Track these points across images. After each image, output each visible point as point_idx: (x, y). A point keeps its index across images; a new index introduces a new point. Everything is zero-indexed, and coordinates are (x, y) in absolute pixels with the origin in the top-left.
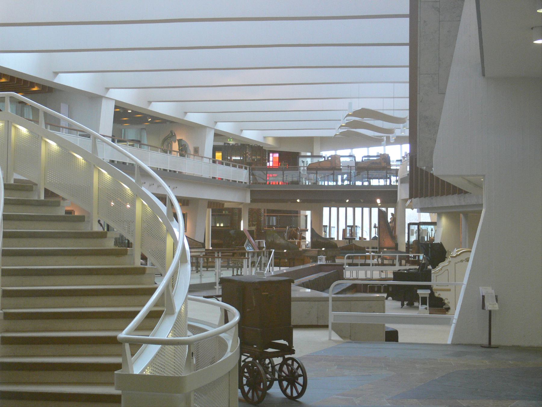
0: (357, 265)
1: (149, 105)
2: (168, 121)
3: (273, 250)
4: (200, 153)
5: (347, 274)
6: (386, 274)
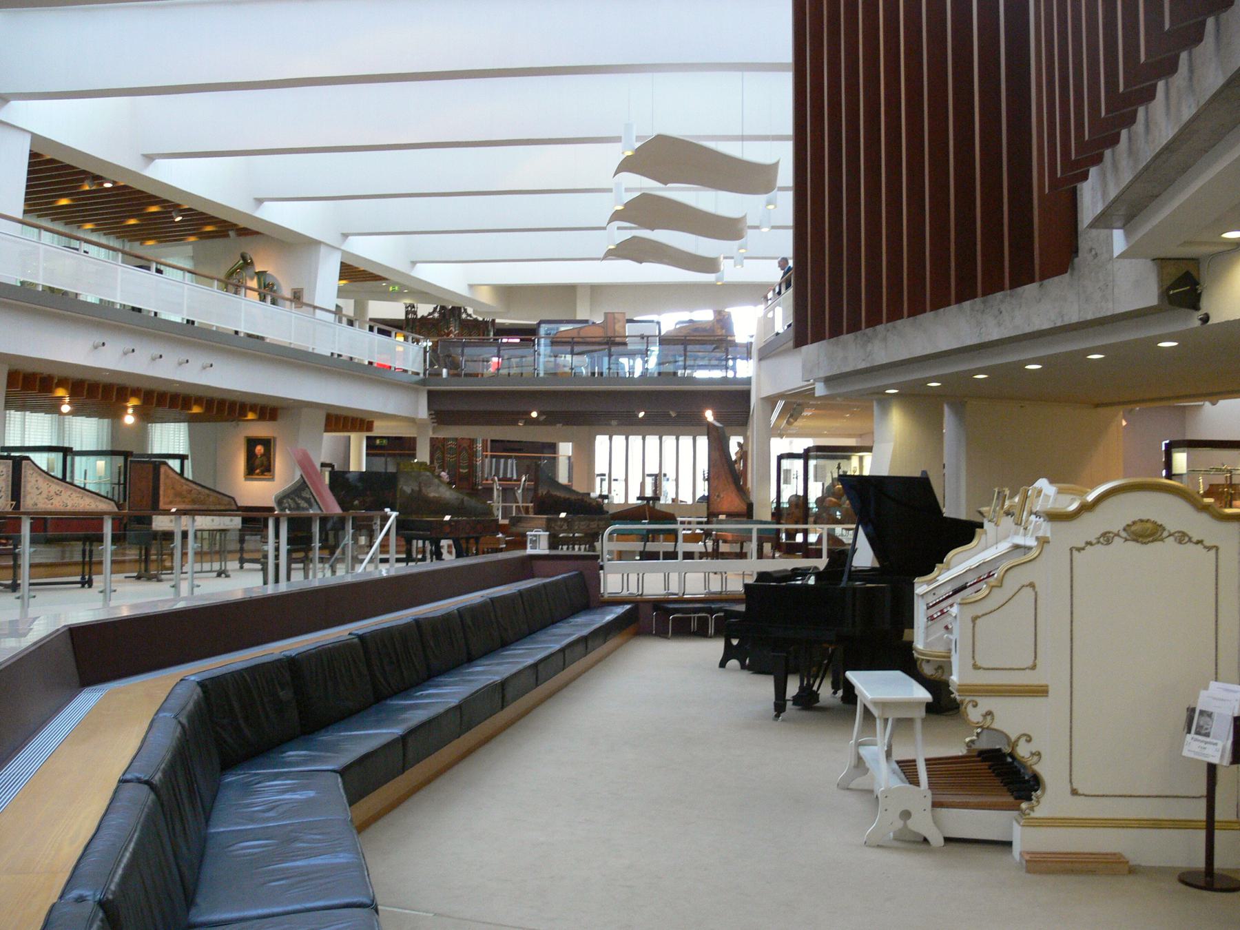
0: (653, 556)
1: (147, 165)
2: (233, 226)
3: (394, 514)
4: (305, 299)
5: (613, 582)
6: (724, 581)
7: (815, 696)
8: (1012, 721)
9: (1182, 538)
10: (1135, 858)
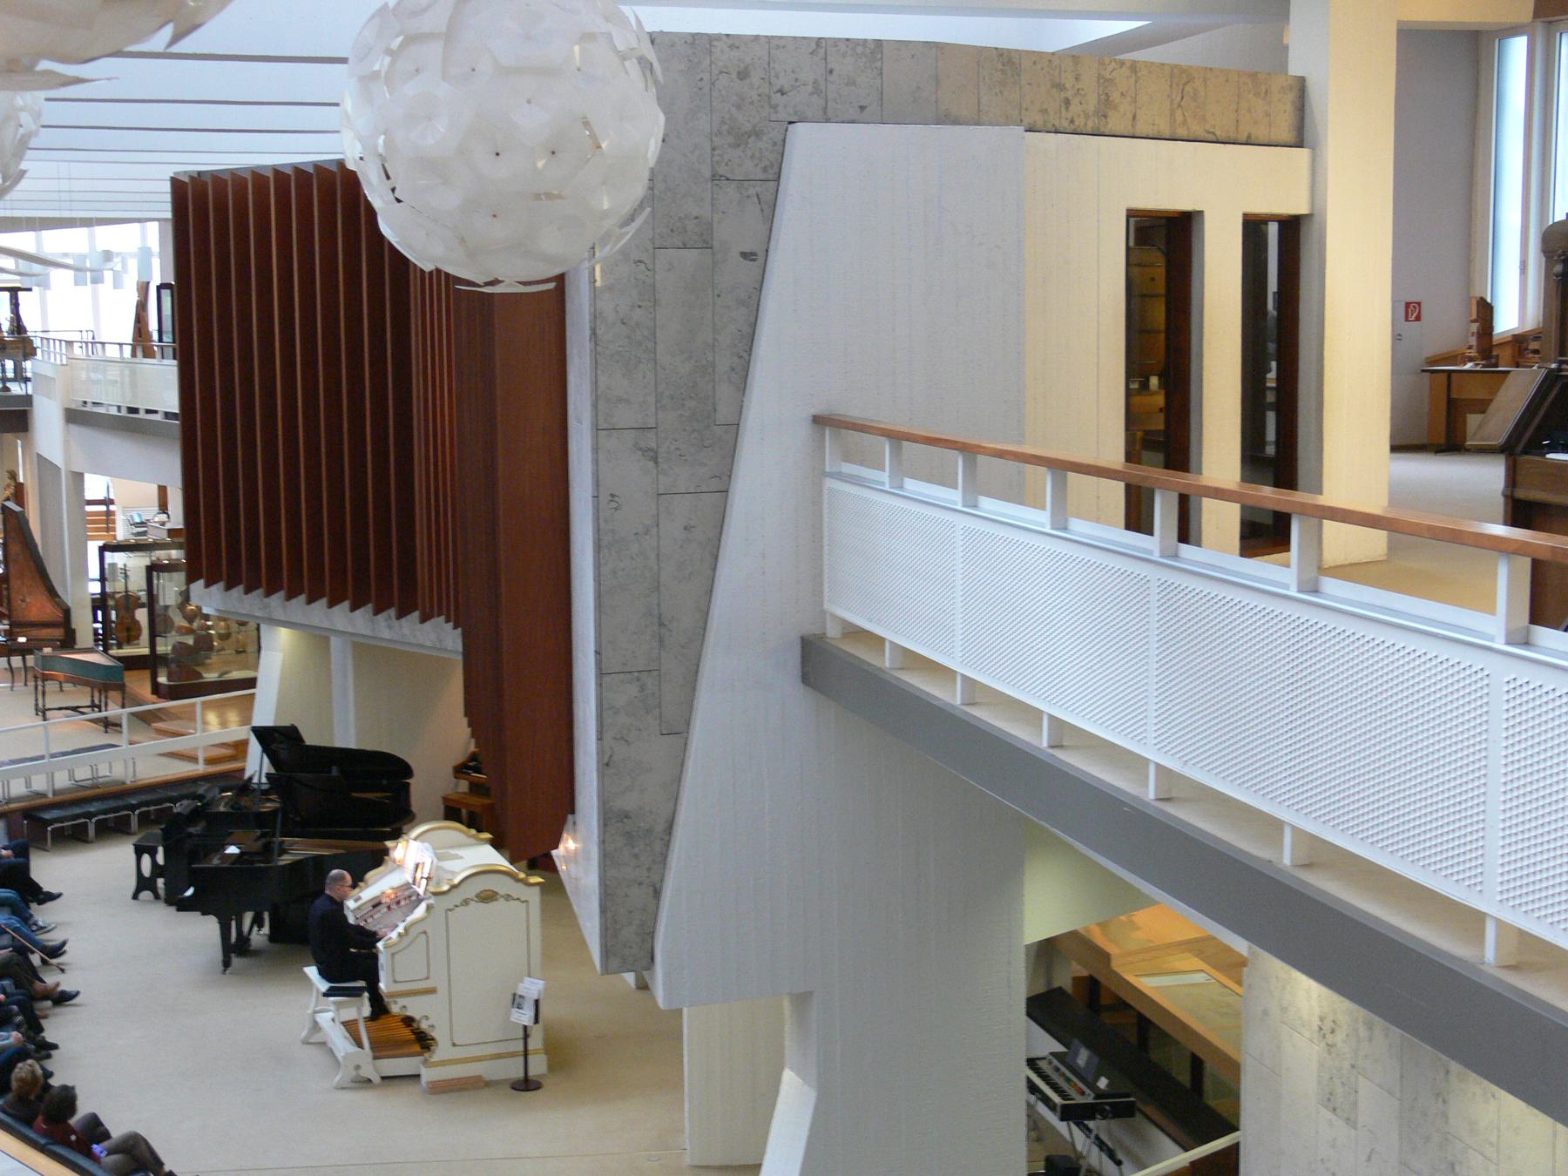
7: (244, 940)
8: (414, 1008)
9: (508, 897)
10: (488, 1076)
